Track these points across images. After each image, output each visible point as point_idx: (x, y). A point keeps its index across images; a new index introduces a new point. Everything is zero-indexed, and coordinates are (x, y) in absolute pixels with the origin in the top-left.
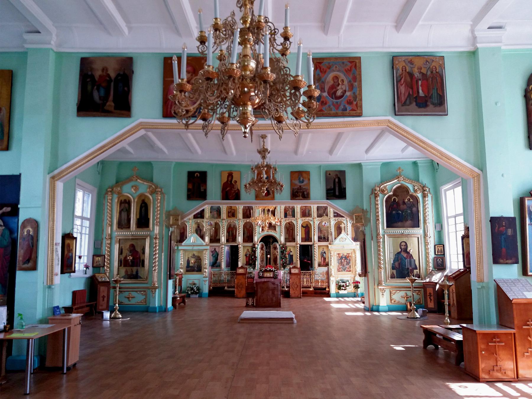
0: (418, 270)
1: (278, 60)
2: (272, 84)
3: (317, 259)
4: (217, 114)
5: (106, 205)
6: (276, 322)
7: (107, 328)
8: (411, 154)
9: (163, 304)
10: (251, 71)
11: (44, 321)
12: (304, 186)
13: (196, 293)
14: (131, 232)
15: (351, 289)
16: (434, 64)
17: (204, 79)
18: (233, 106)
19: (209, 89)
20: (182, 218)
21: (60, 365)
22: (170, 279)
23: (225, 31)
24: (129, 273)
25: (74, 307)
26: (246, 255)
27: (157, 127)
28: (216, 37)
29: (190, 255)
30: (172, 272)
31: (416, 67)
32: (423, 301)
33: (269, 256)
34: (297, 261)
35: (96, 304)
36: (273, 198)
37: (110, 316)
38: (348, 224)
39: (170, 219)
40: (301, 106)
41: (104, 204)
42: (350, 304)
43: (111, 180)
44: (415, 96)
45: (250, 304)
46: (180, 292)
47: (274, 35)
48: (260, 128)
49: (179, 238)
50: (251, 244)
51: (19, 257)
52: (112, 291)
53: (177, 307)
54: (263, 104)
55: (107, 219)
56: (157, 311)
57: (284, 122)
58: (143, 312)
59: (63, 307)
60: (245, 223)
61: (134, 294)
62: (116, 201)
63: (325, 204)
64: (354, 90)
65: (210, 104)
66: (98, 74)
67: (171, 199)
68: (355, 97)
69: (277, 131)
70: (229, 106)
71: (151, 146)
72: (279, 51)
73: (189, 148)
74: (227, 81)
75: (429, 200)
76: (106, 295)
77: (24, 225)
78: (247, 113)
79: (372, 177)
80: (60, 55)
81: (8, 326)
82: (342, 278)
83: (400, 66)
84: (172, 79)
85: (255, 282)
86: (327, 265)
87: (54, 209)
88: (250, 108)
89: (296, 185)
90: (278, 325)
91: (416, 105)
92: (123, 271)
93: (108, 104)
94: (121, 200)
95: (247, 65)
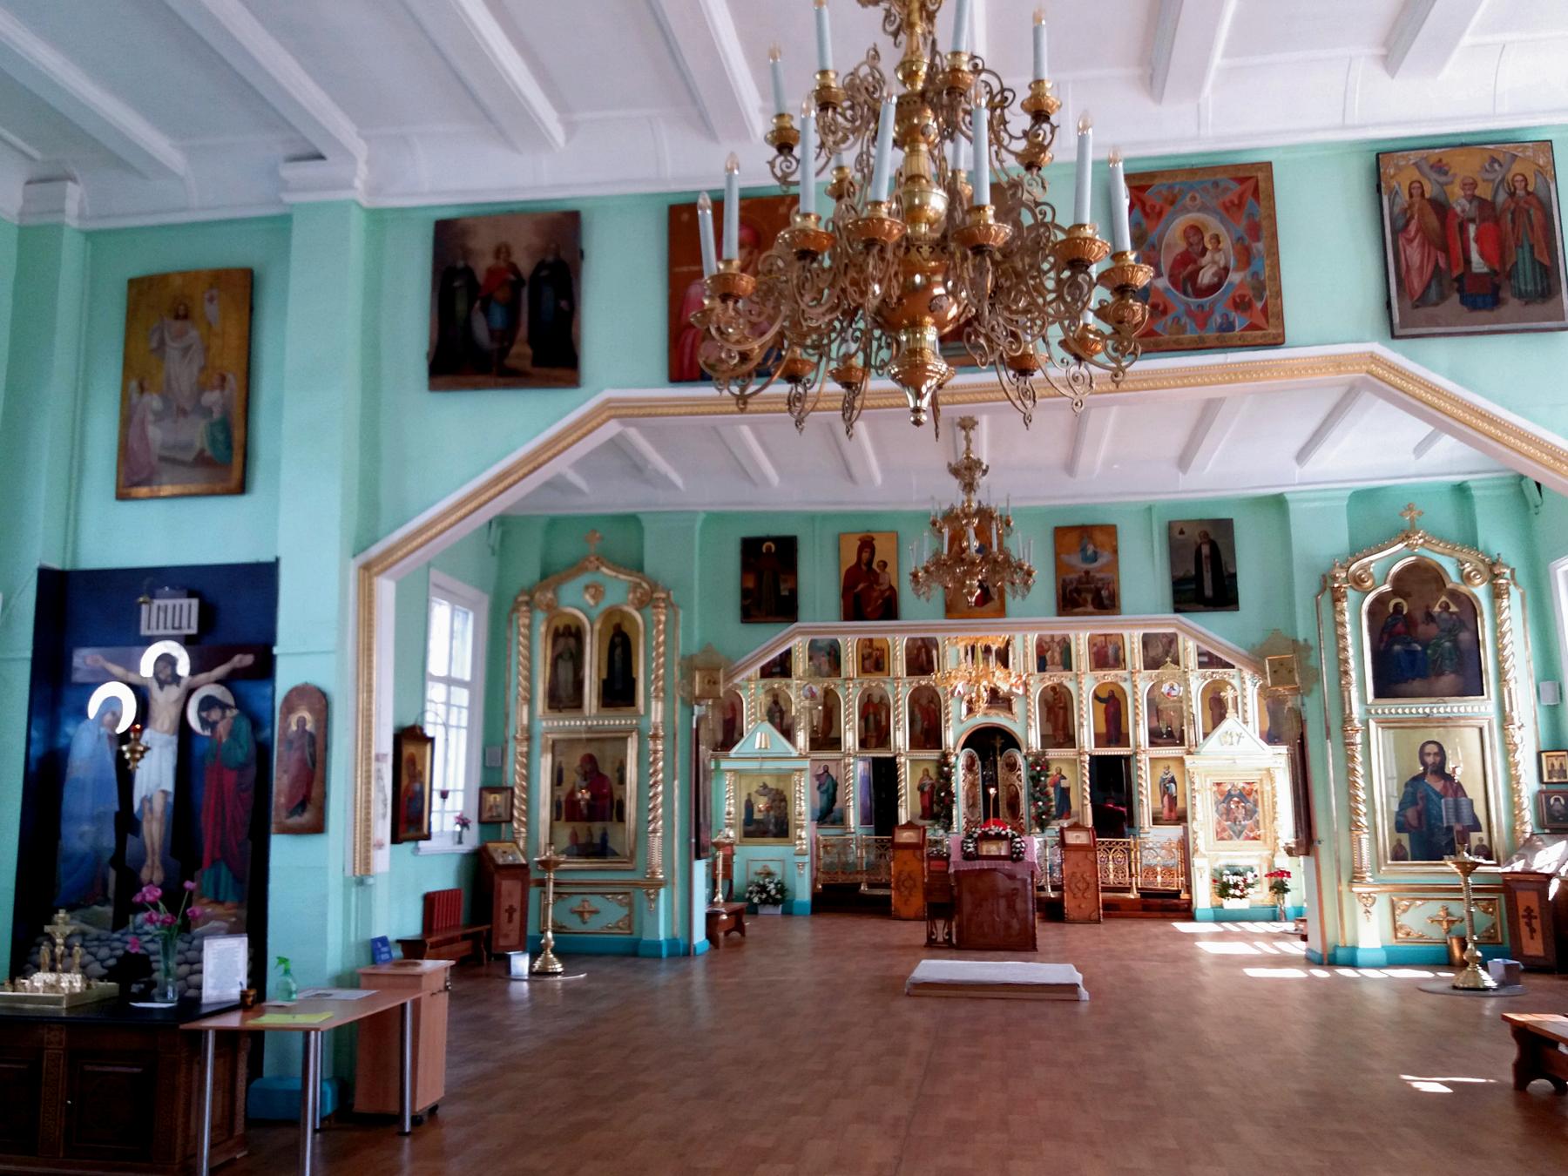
0: (1484, 835)
1: (1016, 185)
2: (998, 256)
3: (1147, 800)
4: (830, 359)
5: (514, 642)
6: (1029, 995)
7: (521, 1002)
8: (1449, 457)
9: (679, 933)
10: (930, 223)
11: (347, 980)
12: (1100, 570)
13: (776, 903)
14: (585, 719)
15: (1260, 895)
16: (1517, 168)
17: (791, 257)
18: (877, 333)
19: (808, 286)
20: (729, 677)
21: (394, 1108)
22: (698, 857)
23: (852, 108)
24: (582, 840)
25: (429, 941)
26: (921, 789)
27: (653, 411)
28: (826, 129)
29: (755, 787)
30: (702, 836)
31: (1458, 181)
32: (1503, 936)
33: (992, 791)
34: (1083, 805)
35: (490, 932)
36: (1001, 612)
37: (531, 966)
38: (1246, 689)
39: (693, 679)
40: (1090, 318)
41: (509, 641)
42: (1258, 944)
43: (529, 572)
44: (1456, 273)
45: (940, 939)
46: (729, 898)
47: (1003, 108)
48: (958, 398)
49: (720, 737)
50: (934, 755)
51: (278, 794)
52: (534, 892)
53: (722, 944)
54: (968, 323)
55: (519, 684)
56: (664, 952)
57: (1038, 374)
58: (624, 955)
59: (398, 941)
60: (916, 690)
61: (596, 902)
62: (543, 629)
63: (1170, 625)
64: (1256, 265)
65: (812, 330)
66: (483, 265)
67: (696, 623)
68: (1259, 289)
69: (1018, 403)
70: (867, 334)
71: (637, 468)
72: (1017, 155)
73: (744, 471)
74: (861, 259)
75: (1513, 605)
76: (517, 905)
77: (290, 705)
78: (922, 349)
79: (1321, 537)
80: (378, 217)
81: (252, 993)
82: (1231, 862)
83: (1401, 183)
84: (695, 268)
85: (951, 870)
86: (1181, 819)
87: (370, 656)
88: (931, 335)
89: (1071, 568)
90: (1028, 1004)
91: (1463, 301)
92: (565, 833)
93: (515, 350)
94: (557, 629)
95: (921, 207)
